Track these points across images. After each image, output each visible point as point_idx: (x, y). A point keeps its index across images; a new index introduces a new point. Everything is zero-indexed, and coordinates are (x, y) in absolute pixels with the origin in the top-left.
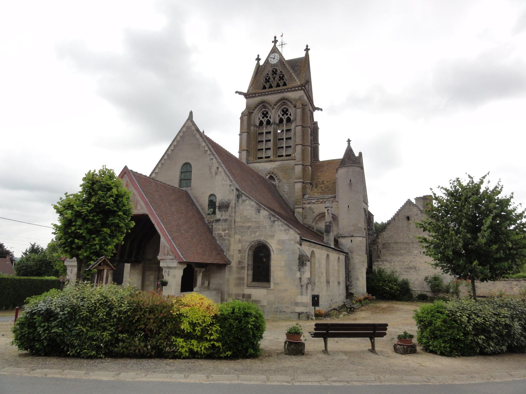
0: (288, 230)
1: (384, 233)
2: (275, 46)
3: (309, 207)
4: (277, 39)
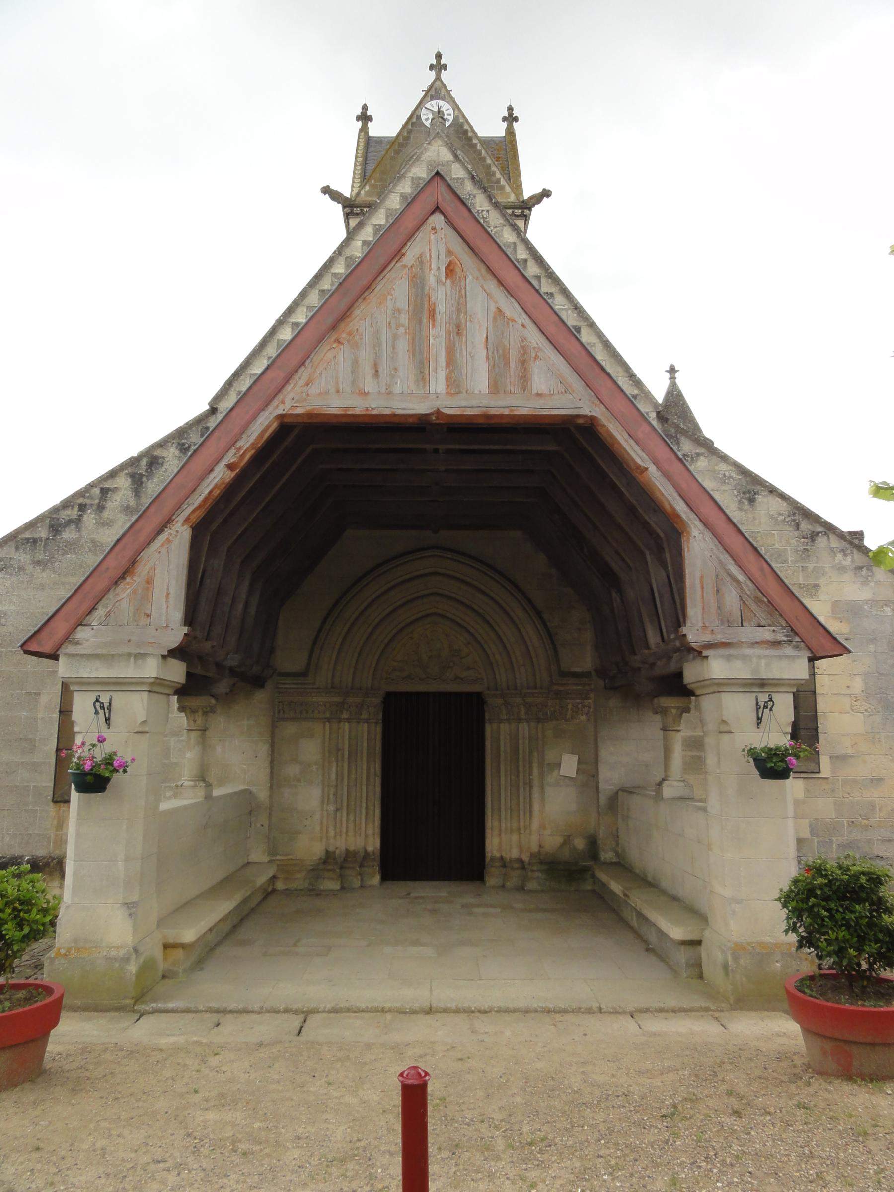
0: (868, 569)
2: (438, 78)
4: (442, 62)
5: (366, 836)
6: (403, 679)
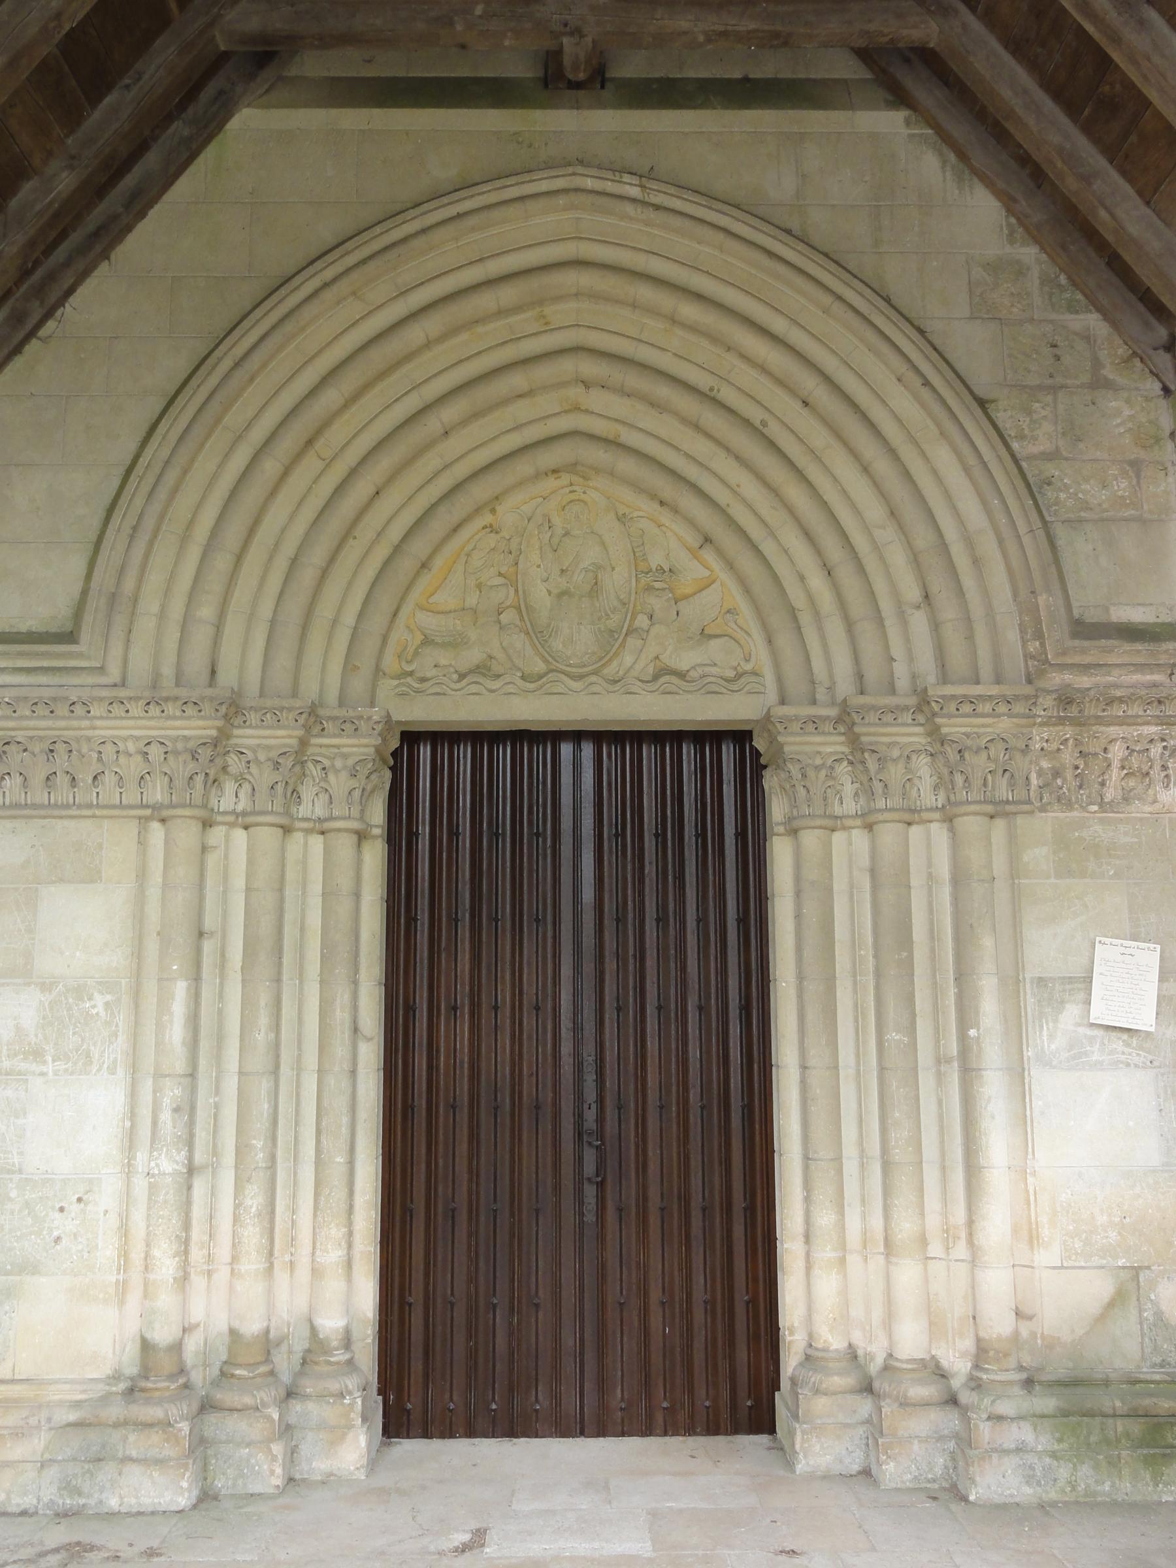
5: (317, 1272)
6: (462, 676)
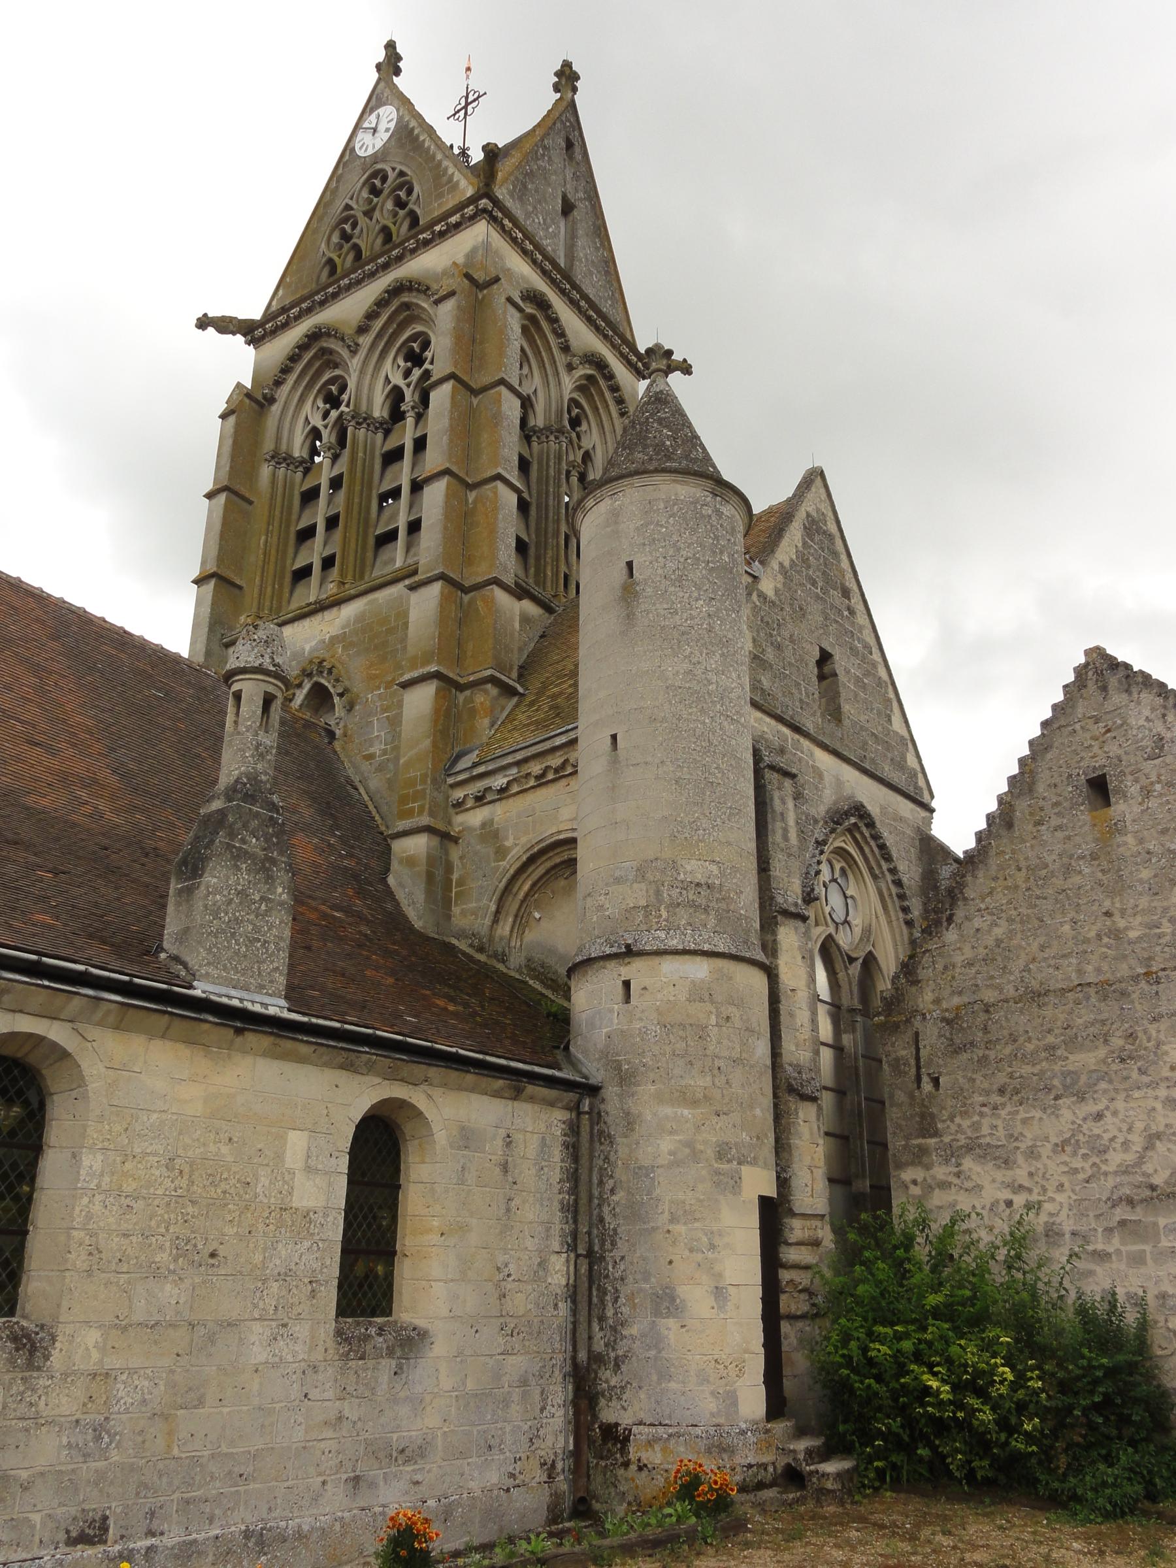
1: (951, 936)
3: (484, 825)
